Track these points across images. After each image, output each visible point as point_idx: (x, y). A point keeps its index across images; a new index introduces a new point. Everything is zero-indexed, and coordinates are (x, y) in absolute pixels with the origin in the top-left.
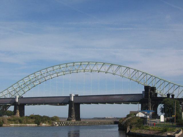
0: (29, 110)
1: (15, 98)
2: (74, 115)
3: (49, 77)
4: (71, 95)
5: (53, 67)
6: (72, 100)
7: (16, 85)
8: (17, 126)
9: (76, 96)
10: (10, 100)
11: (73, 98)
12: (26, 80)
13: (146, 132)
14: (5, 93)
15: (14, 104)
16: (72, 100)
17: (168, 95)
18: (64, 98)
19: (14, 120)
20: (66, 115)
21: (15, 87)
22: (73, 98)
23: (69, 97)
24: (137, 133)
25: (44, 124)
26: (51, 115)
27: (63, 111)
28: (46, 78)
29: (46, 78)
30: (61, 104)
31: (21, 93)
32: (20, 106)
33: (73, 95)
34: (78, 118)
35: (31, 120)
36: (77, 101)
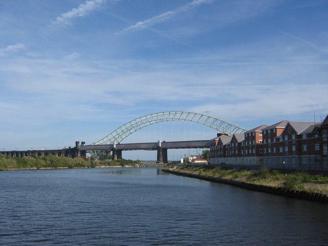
0: (126, 155)
1: (113, 145)
2: (161, 159)
3: (148, 123)
4: (159, 141)
5: (151, 115)
6: (160, 146)
7: (115, 132)
8: (106, 168)
9: (164, 142)
10: (108, 147)
11: (160, 143)
12: (124, 128)
13: (242, 179)
14: (105, 140)
15: (113, 149)
16: (160, 146)
17: (77, 143)
18: (207, 142)
19: (104, 163)
20: (155, 159)
21: (114, 134)
22: (160, 143)
23: (158, 143)
24: (309, 191)
25: (127, 166)
26: (134, 159)
27: (153, 155)
28: (141, 126)
29: (141, 126)
30: (153, 149)
31: (119, 140)
32: (118, 152)
33: (161, 142)
34: (165, 160)
35: (117, 163)
36: (164, 146)
